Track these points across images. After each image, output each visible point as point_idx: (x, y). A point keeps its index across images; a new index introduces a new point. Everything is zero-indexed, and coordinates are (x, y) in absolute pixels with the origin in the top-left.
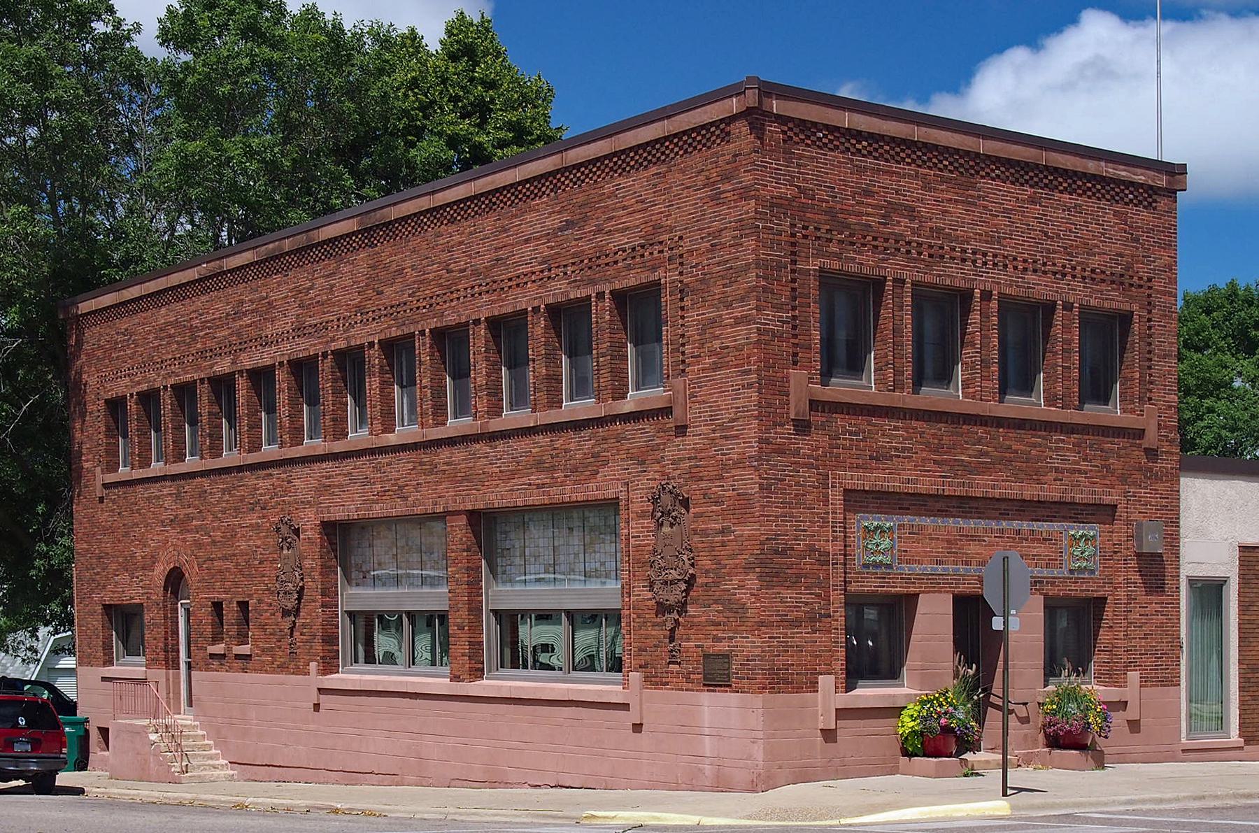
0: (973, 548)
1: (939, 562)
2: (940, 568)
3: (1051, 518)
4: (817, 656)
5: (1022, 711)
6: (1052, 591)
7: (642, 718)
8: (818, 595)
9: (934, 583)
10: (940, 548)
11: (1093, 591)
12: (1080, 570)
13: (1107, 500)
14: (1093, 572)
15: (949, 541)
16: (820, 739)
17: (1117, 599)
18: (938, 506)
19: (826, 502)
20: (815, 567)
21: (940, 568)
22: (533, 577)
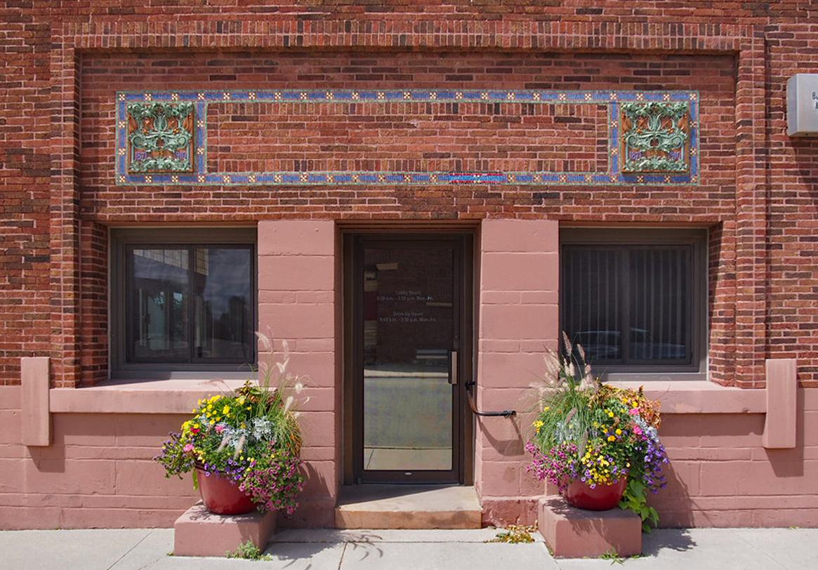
0: (381, 140)
1: (307, 166)
2: (303, 178)
3: (575, 82)
4: (23, 325)
5: (504, 430)
6: (576, 211)
7: (49, 392)
8: (25, 226)
9: (290, 203)
10: (309, 143)
11: (683, 207)
12: (648, 173)
13: (711, 41)
14: (684, 177)
15: (325, 130)
16: (26, 461)
17: (742, 225)
18: (302, 69)
19: (45, 74)
20: (20, 180)
21: (303, 178)
22: (742, 265)
